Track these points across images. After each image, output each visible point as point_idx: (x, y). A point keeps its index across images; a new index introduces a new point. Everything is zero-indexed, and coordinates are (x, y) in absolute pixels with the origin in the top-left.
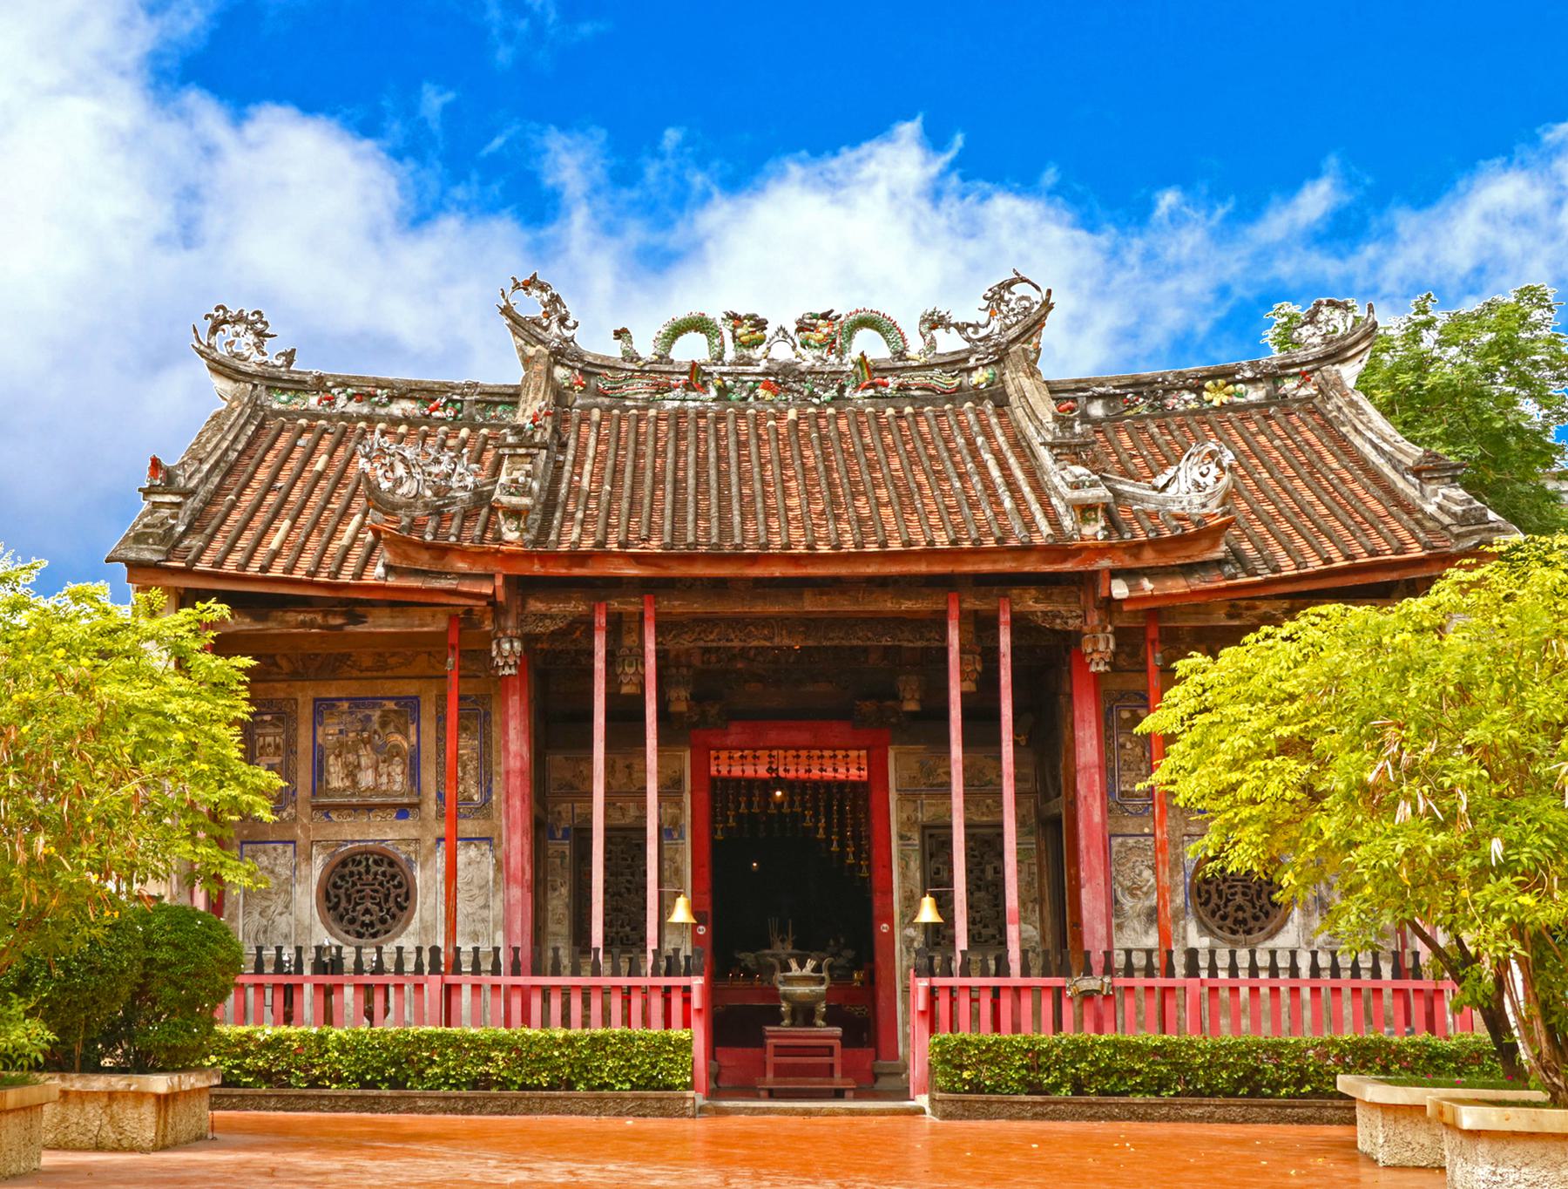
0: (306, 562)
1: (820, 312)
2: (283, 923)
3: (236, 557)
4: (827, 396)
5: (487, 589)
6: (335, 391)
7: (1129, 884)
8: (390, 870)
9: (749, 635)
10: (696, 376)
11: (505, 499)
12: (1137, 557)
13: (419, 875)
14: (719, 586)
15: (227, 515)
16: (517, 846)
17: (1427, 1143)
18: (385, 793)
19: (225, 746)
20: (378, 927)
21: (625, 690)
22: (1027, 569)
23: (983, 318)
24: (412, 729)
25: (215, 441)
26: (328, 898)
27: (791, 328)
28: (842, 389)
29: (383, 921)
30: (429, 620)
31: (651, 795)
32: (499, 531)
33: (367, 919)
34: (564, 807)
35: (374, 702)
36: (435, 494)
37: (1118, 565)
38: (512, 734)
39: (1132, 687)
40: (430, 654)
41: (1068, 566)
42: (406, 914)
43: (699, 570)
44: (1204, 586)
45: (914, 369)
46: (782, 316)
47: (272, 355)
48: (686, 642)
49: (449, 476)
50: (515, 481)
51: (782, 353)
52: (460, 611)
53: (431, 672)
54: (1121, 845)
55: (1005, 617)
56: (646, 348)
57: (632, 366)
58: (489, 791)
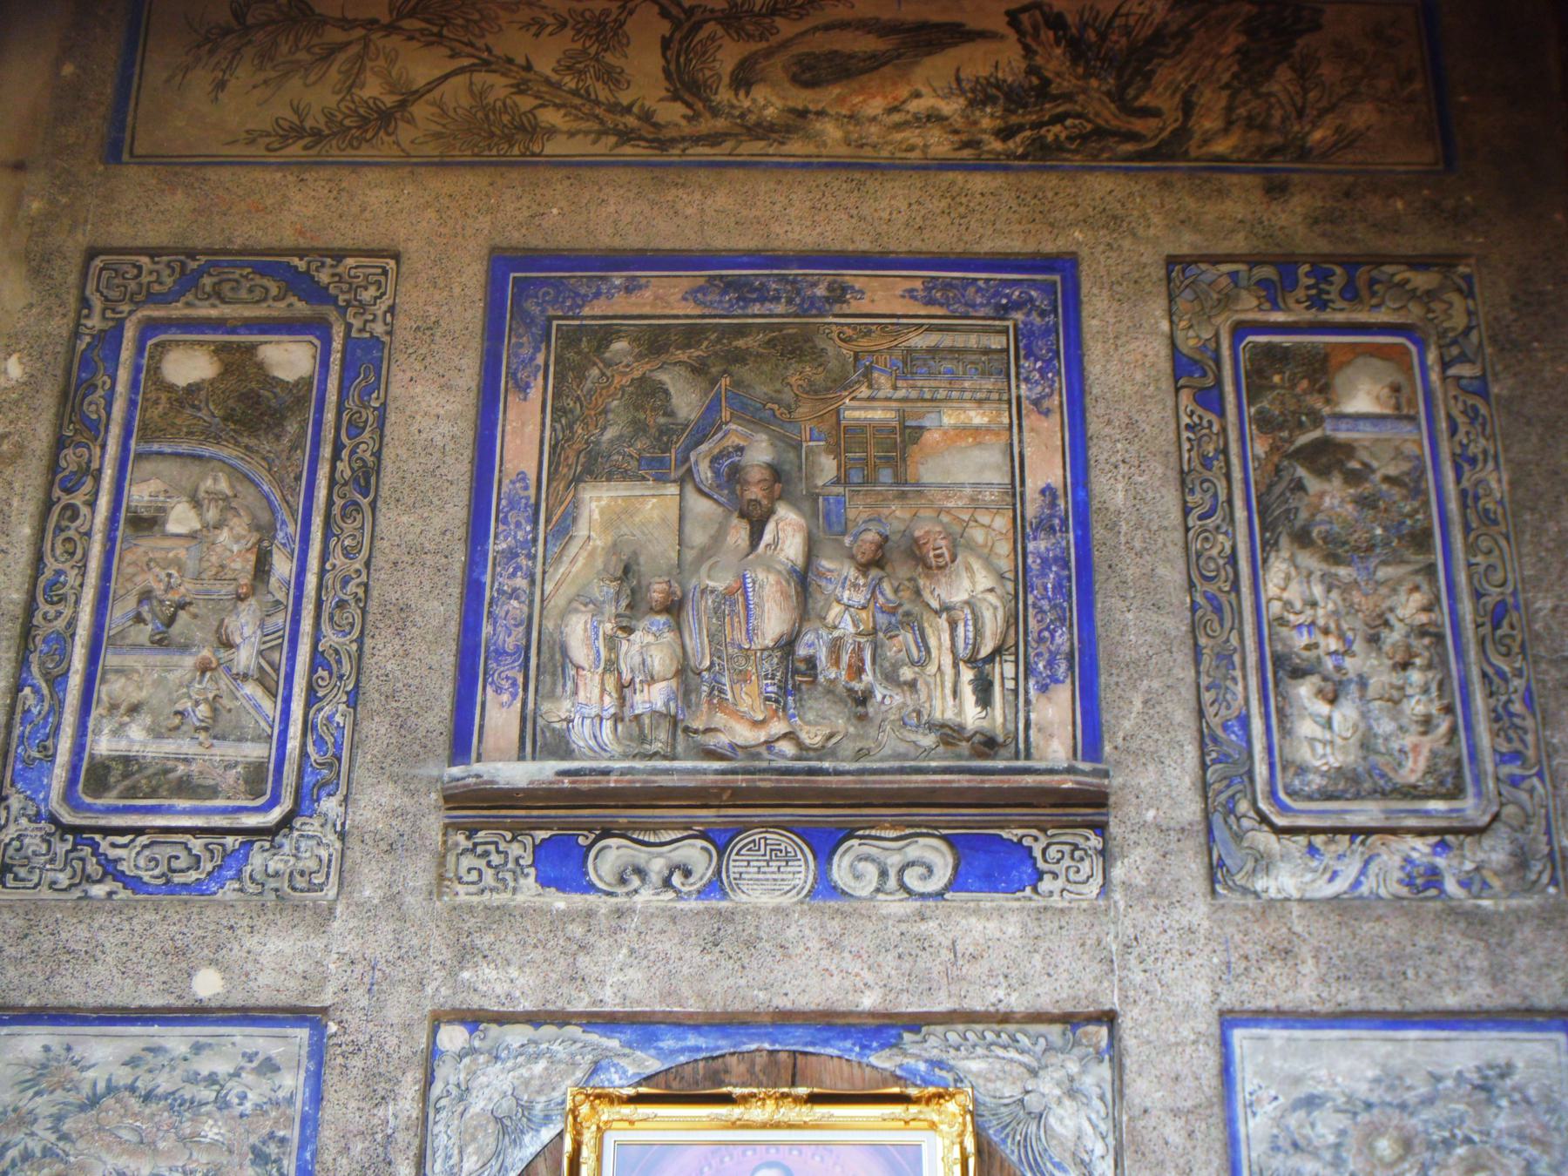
39: (250, 233)
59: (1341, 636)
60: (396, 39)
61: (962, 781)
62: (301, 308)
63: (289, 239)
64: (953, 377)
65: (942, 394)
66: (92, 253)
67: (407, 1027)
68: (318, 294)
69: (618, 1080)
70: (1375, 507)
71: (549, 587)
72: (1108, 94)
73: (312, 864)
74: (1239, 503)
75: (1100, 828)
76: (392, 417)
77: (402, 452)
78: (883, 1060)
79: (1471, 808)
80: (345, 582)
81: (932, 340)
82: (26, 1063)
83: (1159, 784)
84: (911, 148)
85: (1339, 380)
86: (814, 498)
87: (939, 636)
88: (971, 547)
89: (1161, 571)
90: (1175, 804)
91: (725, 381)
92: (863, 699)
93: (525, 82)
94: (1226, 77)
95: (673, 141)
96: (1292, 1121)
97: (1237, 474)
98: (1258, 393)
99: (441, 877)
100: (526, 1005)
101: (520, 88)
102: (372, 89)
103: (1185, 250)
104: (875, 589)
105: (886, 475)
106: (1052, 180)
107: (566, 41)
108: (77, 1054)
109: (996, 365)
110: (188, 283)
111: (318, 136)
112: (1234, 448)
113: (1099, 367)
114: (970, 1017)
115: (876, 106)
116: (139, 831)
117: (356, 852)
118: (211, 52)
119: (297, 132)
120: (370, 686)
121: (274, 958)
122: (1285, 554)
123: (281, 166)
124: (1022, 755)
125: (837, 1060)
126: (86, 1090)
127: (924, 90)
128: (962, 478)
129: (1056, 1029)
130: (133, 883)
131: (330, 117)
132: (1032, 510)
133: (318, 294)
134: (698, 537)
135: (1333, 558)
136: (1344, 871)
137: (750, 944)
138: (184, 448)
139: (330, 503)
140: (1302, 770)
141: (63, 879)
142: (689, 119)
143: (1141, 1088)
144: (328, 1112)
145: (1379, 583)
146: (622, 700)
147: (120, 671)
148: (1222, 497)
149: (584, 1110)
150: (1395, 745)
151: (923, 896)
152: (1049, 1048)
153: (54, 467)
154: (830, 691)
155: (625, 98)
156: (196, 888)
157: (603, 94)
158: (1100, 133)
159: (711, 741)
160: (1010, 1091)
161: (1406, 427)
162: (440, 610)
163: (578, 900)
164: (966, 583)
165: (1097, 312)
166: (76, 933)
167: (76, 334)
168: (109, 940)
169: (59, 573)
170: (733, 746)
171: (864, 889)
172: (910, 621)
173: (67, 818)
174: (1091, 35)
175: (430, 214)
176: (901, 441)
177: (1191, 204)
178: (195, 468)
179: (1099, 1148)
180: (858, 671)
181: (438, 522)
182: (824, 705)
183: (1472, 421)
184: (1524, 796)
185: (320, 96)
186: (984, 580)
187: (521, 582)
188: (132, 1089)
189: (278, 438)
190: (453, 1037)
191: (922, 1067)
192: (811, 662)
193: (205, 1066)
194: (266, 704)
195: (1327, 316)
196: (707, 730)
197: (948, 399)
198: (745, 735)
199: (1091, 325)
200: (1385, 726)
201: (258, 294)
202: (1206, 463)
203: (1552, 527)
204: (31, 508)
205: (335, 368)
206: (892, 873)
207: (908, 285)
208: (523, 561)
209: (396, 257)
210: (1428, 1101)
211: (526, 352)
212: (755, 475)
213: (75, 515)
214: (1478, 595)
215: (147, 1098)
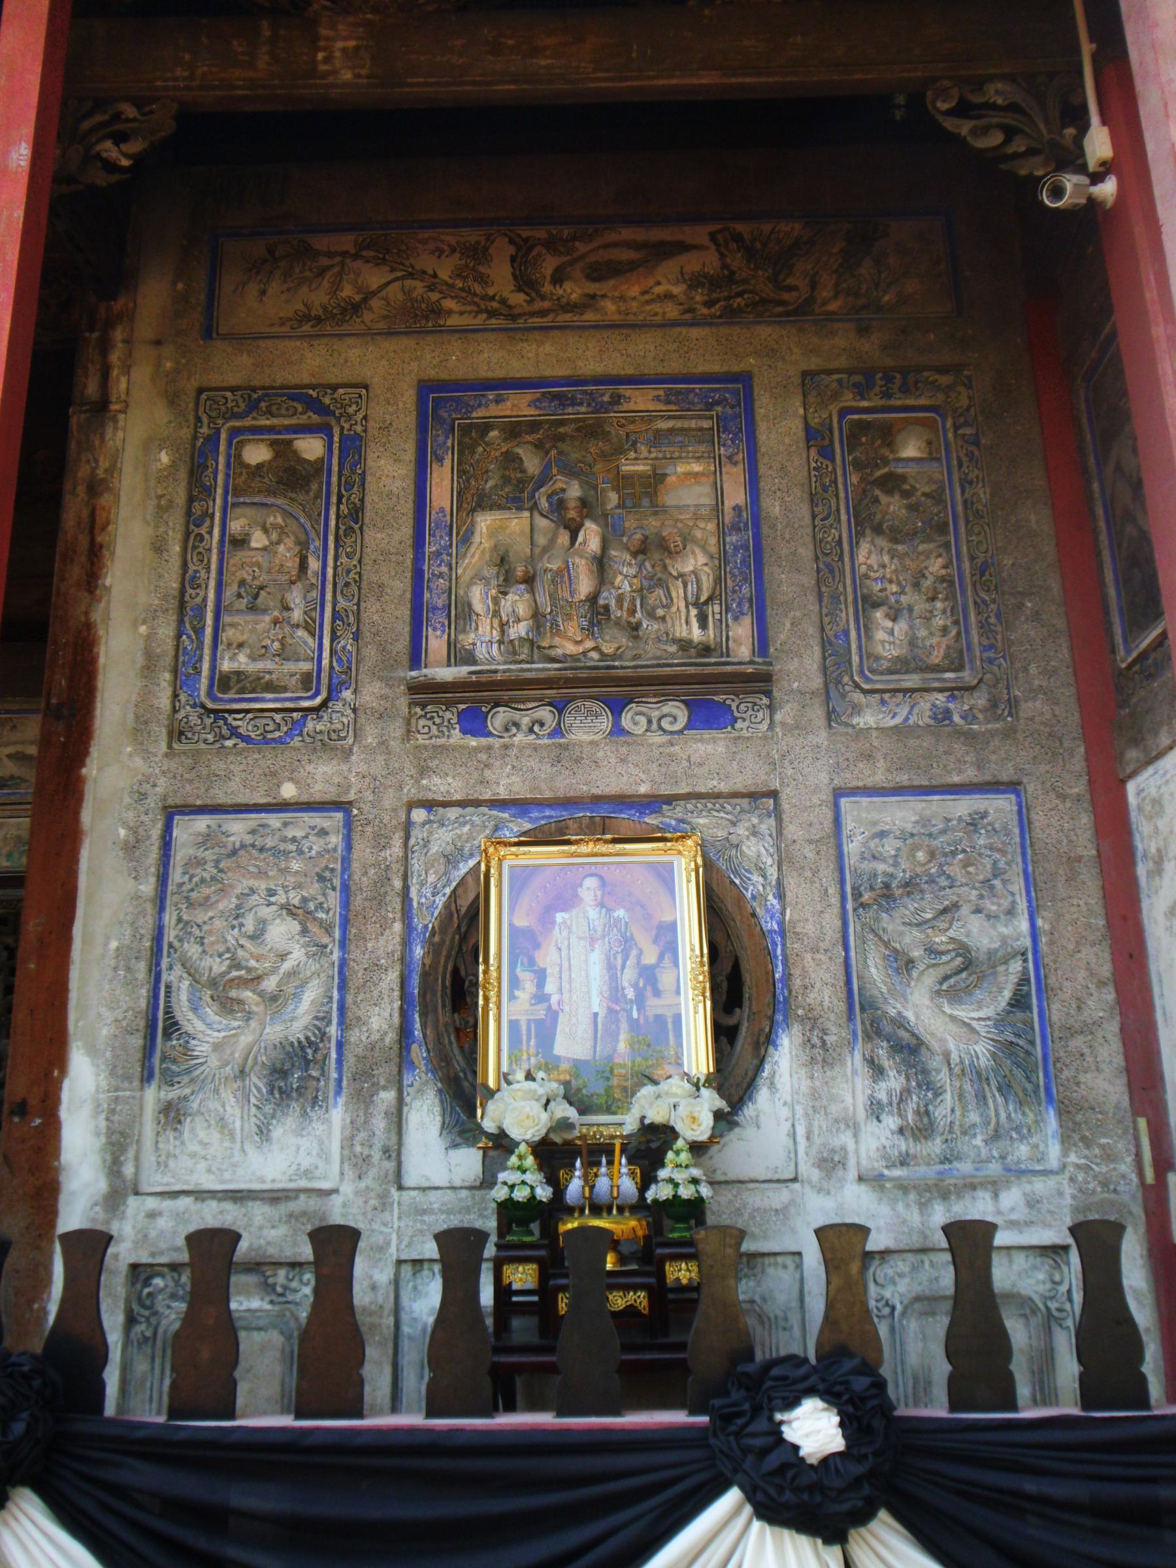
7: (219, 967)
19: (231, 659)
39: (284, 376)
54: (206, 840)
59: (899, 584)
60: (359, 263)
61: (692, 670)
62: (315, 418)
63: (306, 379)
64: (682, 446)
65: (677, 455)
66: (200, 391)
67: (394, 810)
68: (324, 410)
69: (507, 834)
70: (917, 510)
71: (460, 571)
72: (768, 278)
73: (340, 726)
74: (843, 511)
75: (768, 694)
76: (369, 479)
77: (376, 499)
78: (652, 820)
79: (967, 676)
80: (348, 572)
81: (670, 424)
82: (199, 834)
83: (801, 668)
84: (656, 314)
85: (899, 438)
86: (605, 516)
87: (677, 591)
88: (695, 541)
89: (800, 550)
90: (809, 678)
91: (554, 452)
92: (636, 627)
93: (434, 284)
94: (835, 267)
95: (519, 315)
96: (872, 844)
97: (842, 495)
98: (853, 451)
99: (409, 731)
100: (457, 797)
101: (431, 288)
102: (347, 291)
103: (813, 367)
104: (641, 566)
105: (646, 502)
106: (736, 330)
107: (456, 260)
108: (223, 829)
109: (704, 436)
110: (253, 406)
111: (319, 320)
112: (840, 480)
113: (766, 437)
114: (698, 796)
115: (635, 291)
116: (248, 711)
117: (362, 718)
118: (257, 273)
119: (307, 318)
120: (365, 629)
121: (322, 776)
122: (869, 539)
123: (299, 337)
125: (626, 820)
126: (230, 847)
127: (663, 280)
128: (688, 502)
129: (746, 801)
130: (247, 739)
131: (325, 308)
132: (727, 519)
133: (324, 410)
134: (542, 541)
135: (896, 541)
136: (899, 714)
137: (577, 761)
138: (257, 500)
139: (337, 528)
140: (878, 658)
141: (210, 738)
142: (529, 302)
143: (792, 830)
144: (355, 854)
145: (920, 554)
146: (503, 632)
147: (232, 625)
148: (834, 508)
149: (491, 850)
150: (928, 643)
151: (672, 733)
152: (742, 811)
153: (189, 513)
154: (618, 623)
155: (491, 292)
156: (279, 741)
157: (478, 289)
158: (764, 301)
159: (552, 653)
160: (721, 834)
161: (935, 464)
162: (401, 586)
163: (484, 741)
164: (692, 561)
165: (764, 405)
166: (219, 766)
167: (195, 438)
168: (236, 768)
169: (196, 572)
170: (565, 655)
171: (639, 730)
172: (661, 583)
173: (210, 705)
174: (758, 245)
175: (384, 362)
176: (655, 482)
177: (815, 340)
178: (264, 511)
179: (769, 861)
180: (632, 612)
181: (397, 537)
182: (615, 631)
183: (971, 460)
184: (996, 669)
185: (318, 297)
186: (702, 559)
187: (444, 569)
188: (253, 846)
189: (307, 492)
190: (419, 815)
191: (673, 822)
192: (607, 608)
193: (290, 833)
194: (310, 640)
195: (892, 402)
196: (550, 647)
197: (680, 458)
198: (571, 649)
199: (760, 412)
200: (922, 633)
201: (291, 412)
202: (825, 490)
203: (1013, 519)
204: (179, 536)
205: (336, 452)
206: (655, 721)
207: (656, 393)
208: (445, 557)
209: (366, 387)
210: (943, 832)
211: (441, 439)
212: (572, 504)
213: (202, 539)
214: (972, 558)
215: (262, 850)
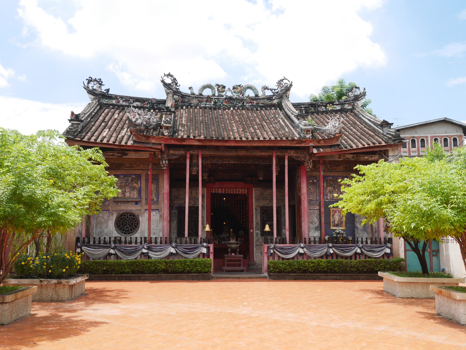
0: (112, 139)
1: (238, 85)
2: (106, 231)
3: (94, 138)
4: (240, 105)
5: (160, 147)
6: (120, 99)
8: (133, 217)
9: (224, 160)
10: (209, 99)
11: (165, 125)
12: (319, 143)
13: (141, 219)
14: (217, 148)
15: (92, 127)
16: (166, 211)
17: (410, 292)
18: (132, 198)
20: (130, 231)
21: (193, 173)
22: (293, 145)
23: (276, 88)
24: (139, 182)
25: (89, 110)
26: (117, 224)
27: (231, 88)
28: (243, 103)
29: (131, 230)
30: (144, 155)
31: (199, 199)
32: (163, 132)
33: (127, 229)
34: (176, 202)
35: (129, 175)
36: (146, 123)
37: (315, 145)
38: (165, 184)
40: (144, 164)
41: (303, 145)
42: (137, 228)
43: (213, 144)
44: (334, 150)
45: (260, 99)
46: (229, 85)
47: (103, 89)
48: (208, 162)
49: (149, 119)
50: (167, 120)
51: (229, 94)
52: (152, 153)
53: (144, 168)
55: (287, 157)
56: (197, 92)
57: (192, 96)
58: (158, 198)
124: (378, 242)
